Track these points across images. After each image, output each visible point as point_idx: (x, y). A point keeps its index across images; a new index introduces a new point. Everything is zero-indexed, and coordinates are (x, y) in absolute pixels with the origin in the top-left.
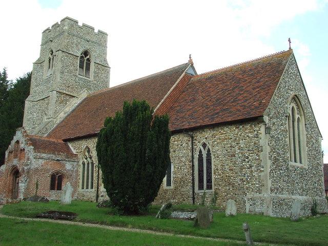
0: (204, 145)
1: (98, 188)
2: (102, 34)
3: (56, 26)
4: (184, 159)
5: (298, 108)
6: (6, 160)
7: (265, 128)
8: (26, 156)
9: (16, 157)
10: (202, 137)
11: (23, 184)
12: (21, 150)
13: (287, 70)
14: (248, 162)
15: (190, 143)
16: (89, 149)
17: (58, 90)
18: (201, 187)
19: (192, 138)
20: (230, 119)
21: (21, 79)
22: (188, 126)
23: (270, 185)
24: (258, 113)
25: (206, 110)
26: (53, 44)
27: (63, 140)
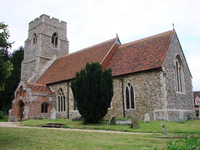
0: (129, 84)
1: (68, 111)
2: (64, 23)
3: (37, 20)
5: (179, 62)
6: (15, 97)
7: (163, 74)
8: (27, 94)
9: (21, 95)
10: (127, 80)
11: (27, 110)
12: (24, 91)
13: (173, 41)
14: (154, 92)
15: (121, 83)
16: (62, 89)
17: (41, 56)
18: (128, 108)
19: (122, 80)
20: (143, 69)
21: (17, 51)
23: (166, 105)
24: (158, 65)
25: (129, 65)
26: (36, 30)
27: (46, 85)
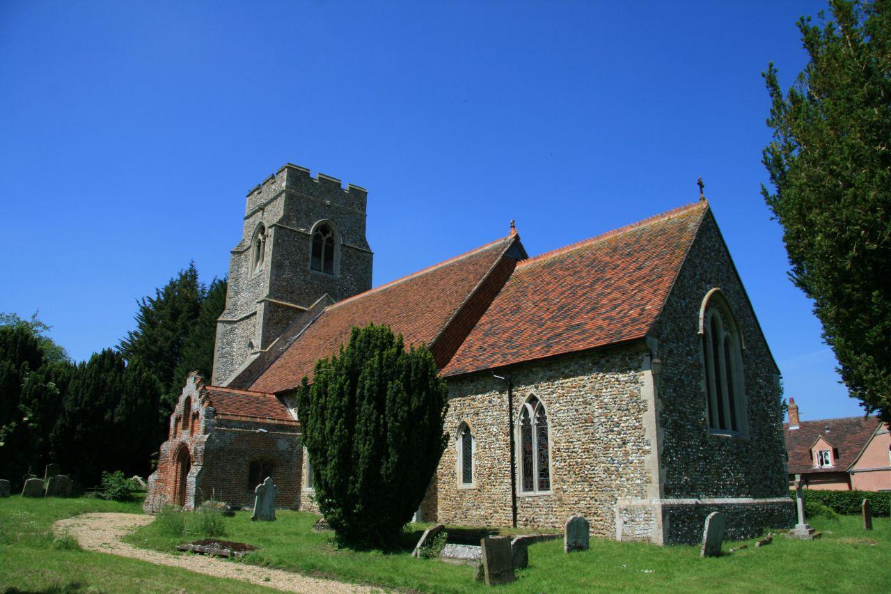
4: (494, 429)
5: (725, 318)
6: (172, 432)
18: (528, 486)
20: (580, 347)
22: (502, 362)
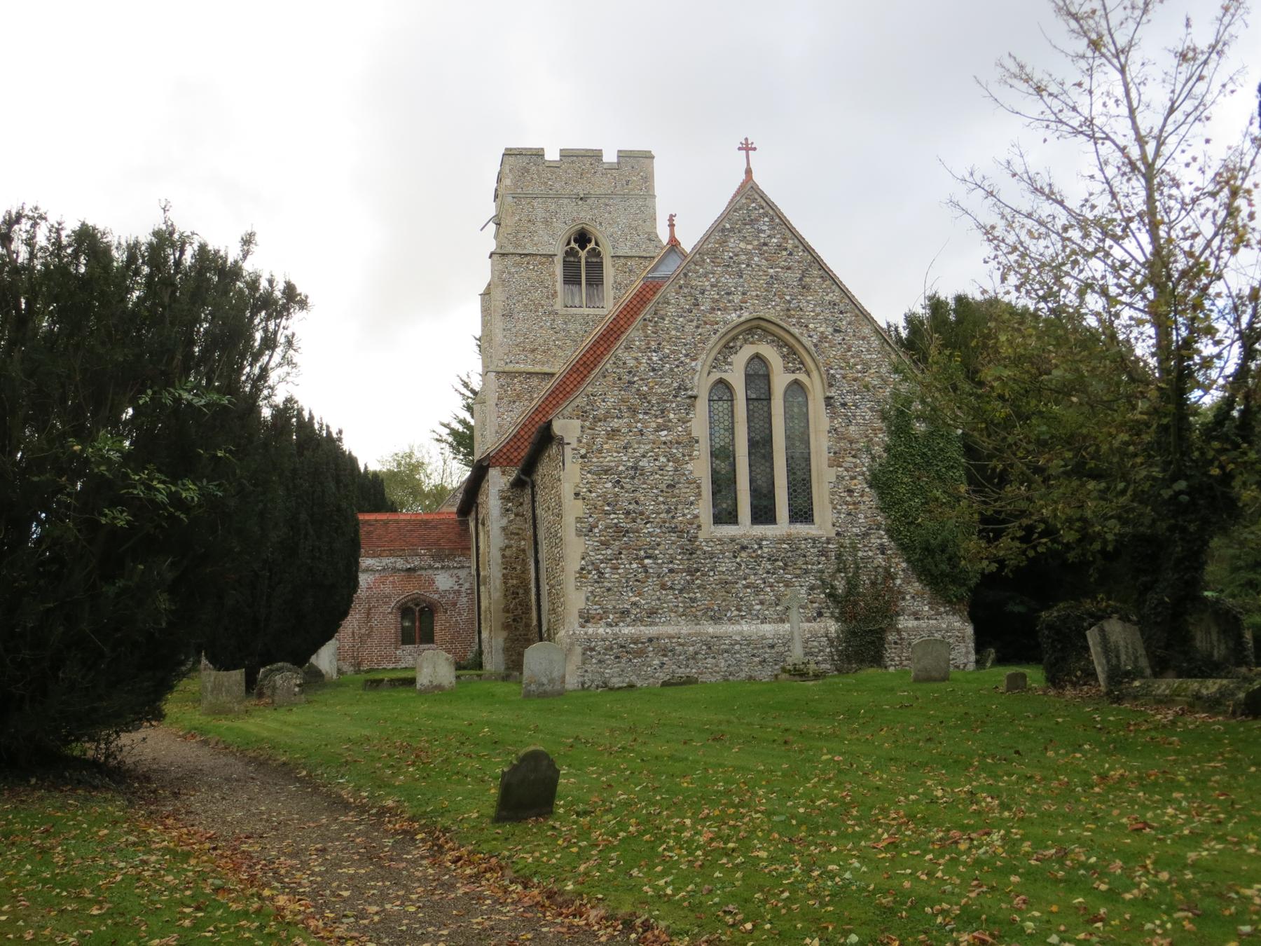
21: (936, 305)
